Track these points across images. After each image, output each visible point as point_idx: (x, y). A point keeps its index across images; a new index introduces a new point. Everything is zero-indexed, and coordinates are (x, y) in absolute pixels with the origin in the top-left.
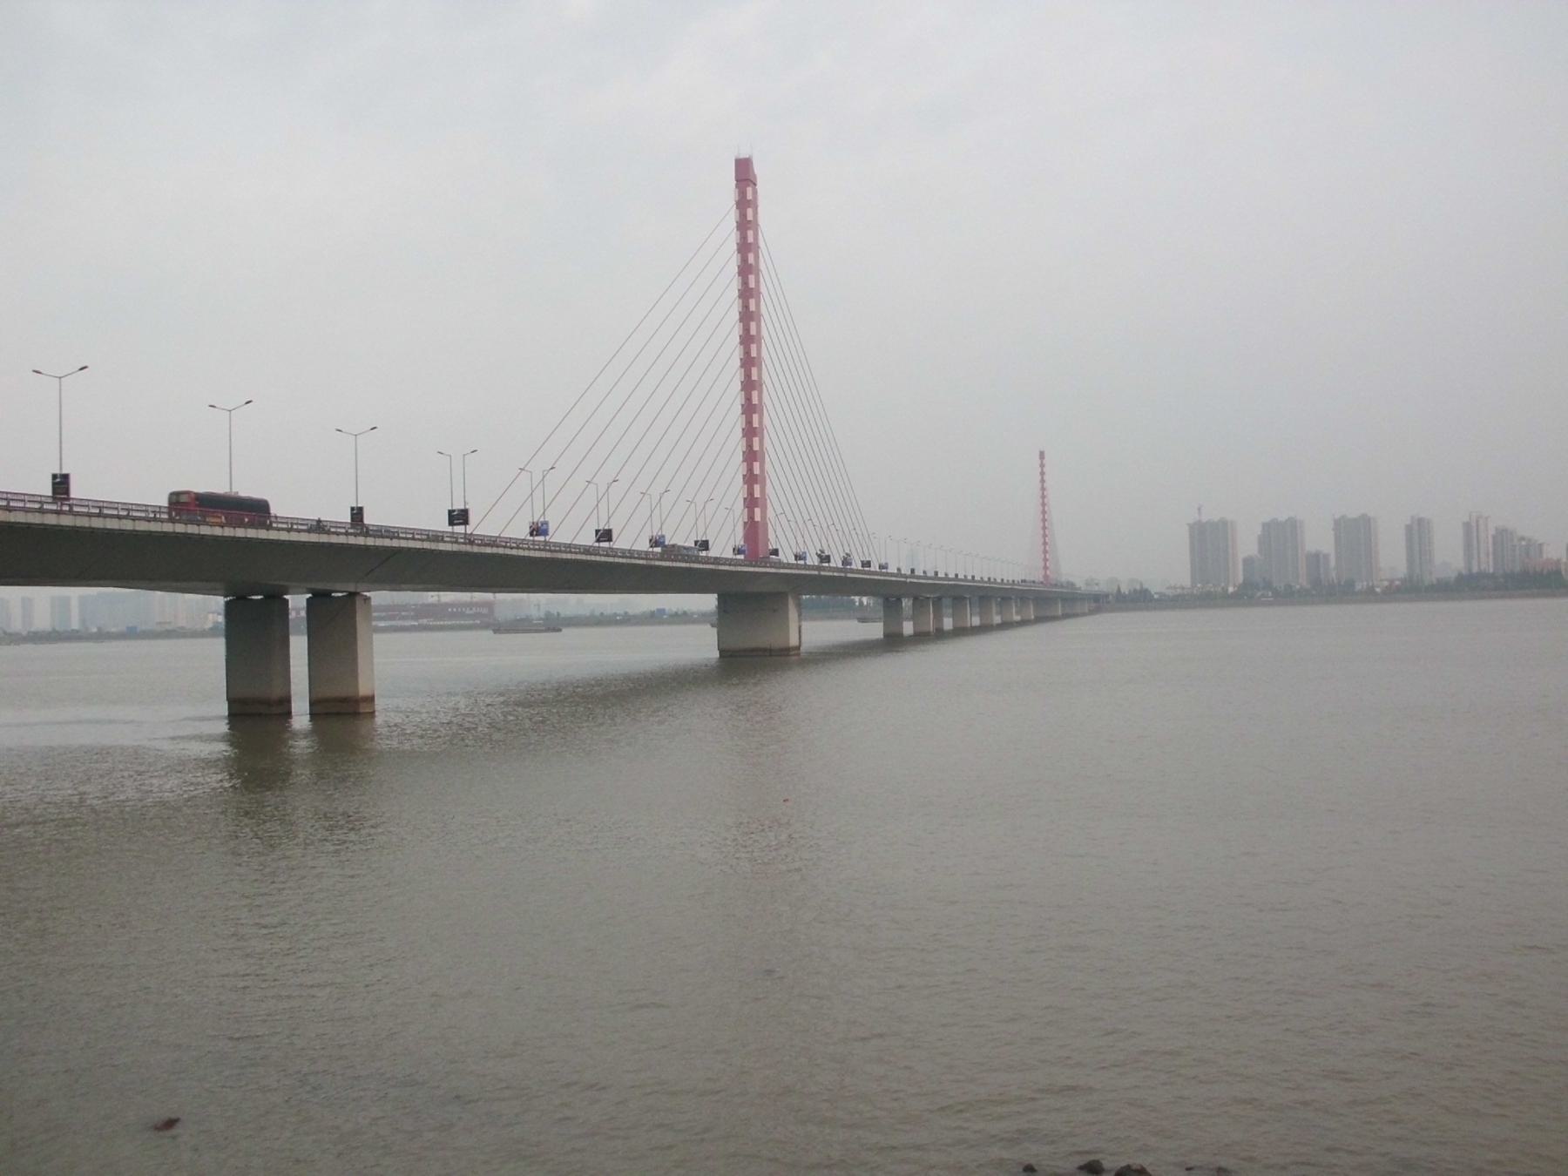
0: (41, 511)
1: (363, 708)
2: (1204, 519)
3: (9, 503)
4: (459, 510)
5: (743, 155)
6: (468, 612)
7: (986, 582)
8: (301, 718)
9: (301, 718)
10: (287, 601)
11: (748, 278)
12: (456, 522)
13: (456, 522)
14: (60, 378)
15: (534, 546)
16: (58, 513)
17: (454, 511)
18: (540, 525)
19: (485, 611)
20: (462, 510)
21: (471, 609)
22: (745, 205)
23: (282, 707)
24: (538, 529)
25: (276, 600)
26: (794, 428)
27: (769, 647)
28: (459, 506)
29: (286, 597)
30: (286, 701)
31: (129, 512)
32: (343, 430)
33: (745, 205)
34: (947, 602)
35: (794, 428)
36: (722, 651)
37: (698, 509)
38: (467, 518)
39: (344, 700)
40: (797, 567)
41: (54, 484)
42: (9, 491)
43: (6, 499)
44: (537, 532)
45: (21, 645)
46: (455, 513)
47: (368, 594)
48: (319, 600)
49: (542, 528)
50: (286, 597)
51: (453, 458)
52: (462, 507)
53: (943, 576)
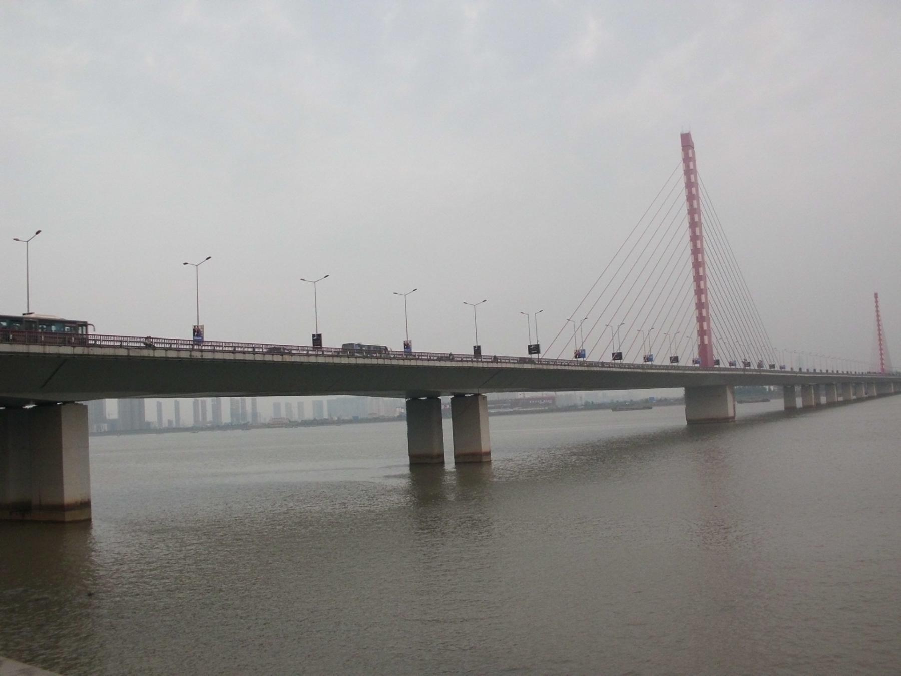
0: (308, 355)
1: (484, 459)
4: (534, 345)
5: (685, 131)
6: (541, 402)
17: (531, 346)
18: (580, 351)
19: (550, 402)
20: (535, 345)
21: (542, 401)
24: (579, 354)
28: (534, 343)
29: (439, 397)
30: (441, 456)
36: (689, 421)
39: (473, 454)
40: (673, 367)
41: (313, 340)
44: (579, 355)
46: (532, 347)
48: (458, 399)
50: (439, 397)
52: (536, 343)
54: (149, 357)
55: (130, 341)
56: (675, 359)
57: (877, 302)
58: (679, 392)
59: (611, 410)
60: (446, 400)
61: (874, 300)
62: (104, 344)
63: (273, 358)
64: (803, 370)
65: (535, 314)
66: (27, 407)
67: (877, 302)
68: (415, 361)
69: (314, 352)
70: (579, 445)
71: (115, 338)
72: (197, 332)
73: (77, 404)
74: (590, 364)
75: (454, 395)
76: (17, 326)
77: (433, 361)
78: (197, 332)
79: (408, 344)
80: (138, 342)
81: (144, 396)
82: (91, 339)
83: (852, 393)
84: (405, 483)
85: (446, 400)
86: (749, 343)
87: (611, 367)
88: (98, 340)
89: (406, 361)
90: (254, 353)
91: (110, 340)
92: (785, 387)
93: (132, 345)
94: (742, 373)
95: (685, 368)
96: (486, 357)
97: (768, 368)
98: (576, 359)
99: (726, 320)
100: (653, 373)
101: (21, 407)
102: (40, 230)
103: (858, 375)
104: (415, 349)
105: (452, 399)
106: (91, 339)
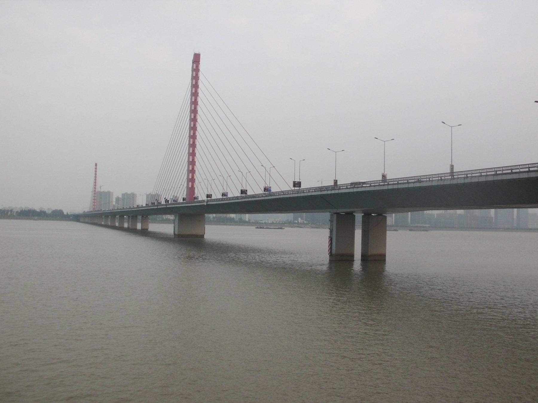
0: (379, 185)
2: (102, 191)
3: (481, 174)
4: (298, 182)
7: (116, 210)
8: (357, 265)
9: (357, 265)
10: (355, 216)
11: (197, 98)
12: (296, 186)
13: (296, 186)
14: (336, 152)
15: (298, 192)
16: (384, 185)
17: (296, 182)
18: (268, 188)
20: (299, 182)
22: (196, 70)
23: (350, 258)
24: (243, 192)
25: (350, 216)
26: (175, 168)
27: (196, 234)
28: (297, 180)
30: (353, 256)
31: (370, 183)
32: (331, 149)
33: (196, 70)
34: (140, 217)
35: (175, 168)
37: (206, 185)
38: (301, 185)
40: (224, 200)
42: (433, 174)
43: (479, 173)
44: (267, 190)
45: (59, 209)
46: (296, 183)
47: (385, 215)
48: (367, 216)
49: (269, 189)
51: (296, 161)
52: (299, 181)
53: (133, 207)
54: (441, 185)
55: (521, 168)
56: (297, 184)
57: (96, 168)
58: (171, 217)
59: (409, 231)
60: (359, 217)
61: (94, 167)
62: (499, 173)
63: (398, 186)
64: (131, 207)
65: (270, 168)
66: (373, 215)
67: (96, 168)
68: (338, 190)
69: (383, 184)
70: (258, 249)
71: (529, 165)
72: (384, 176)
73: (341, 214)
74: (230, 199)
75: (364, 214)
76: (266, 193)
77: (349, 189)
78: (384, 176)
79: (385, 176)
80: (402, 180)
81: (514, 206)
82: (455, 175)
83: (494, 219)
84: (325, 268)
85: (359, 217)
86: (165, 188)
87: (239, 199)
88: (431, 178)
89: (354, 189)
90: (408, 183)
91: (477, 173)
92: (143, 216)
93: (490, 174)
94: (165, 207)
95: (217, 200)
96: (403, 179)
97: (182, 201)
98: (264, 192)
99: (170, 174)
100: (231, 203)
101: (371, 214)
102: (441, 122)
103: (120, 210)
104: (388, 177)
105: (363, 216)
106: (455, 175)
